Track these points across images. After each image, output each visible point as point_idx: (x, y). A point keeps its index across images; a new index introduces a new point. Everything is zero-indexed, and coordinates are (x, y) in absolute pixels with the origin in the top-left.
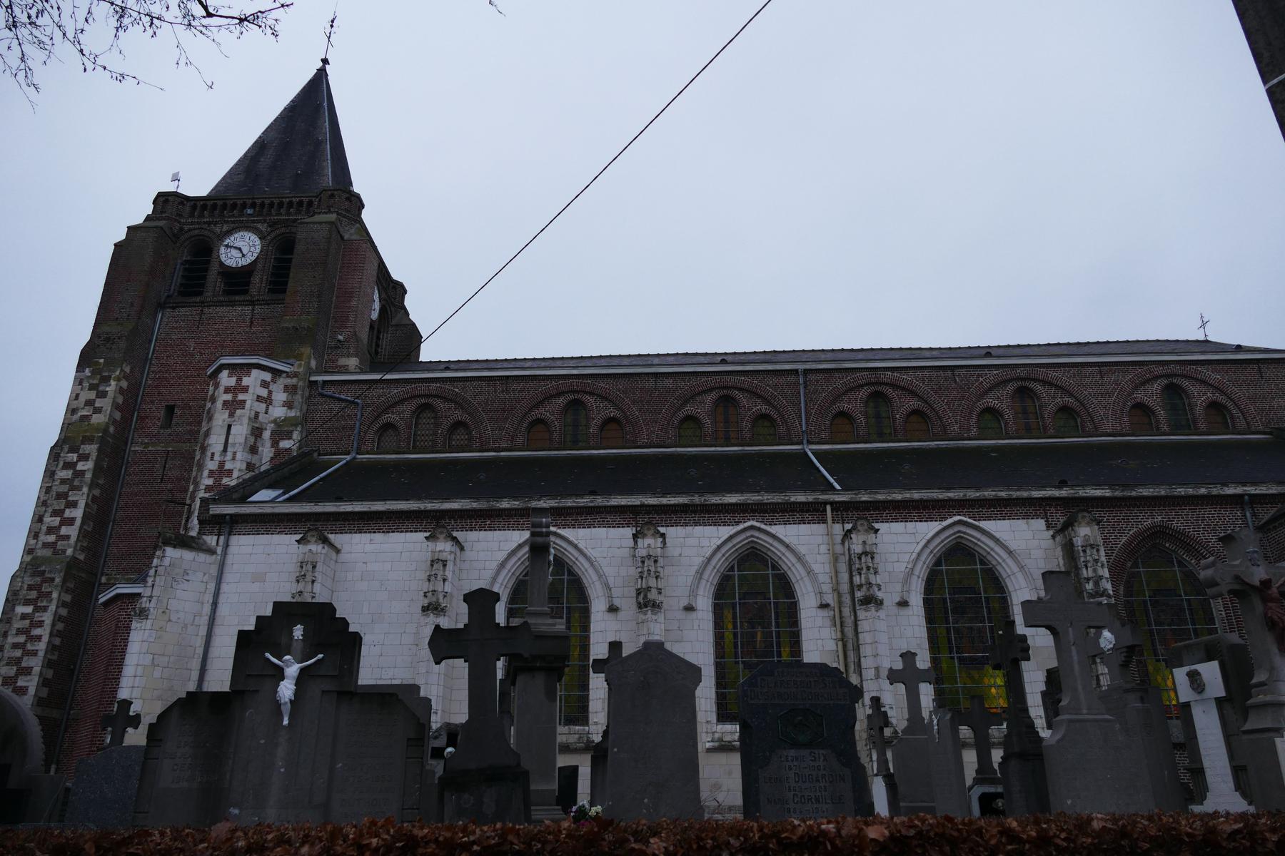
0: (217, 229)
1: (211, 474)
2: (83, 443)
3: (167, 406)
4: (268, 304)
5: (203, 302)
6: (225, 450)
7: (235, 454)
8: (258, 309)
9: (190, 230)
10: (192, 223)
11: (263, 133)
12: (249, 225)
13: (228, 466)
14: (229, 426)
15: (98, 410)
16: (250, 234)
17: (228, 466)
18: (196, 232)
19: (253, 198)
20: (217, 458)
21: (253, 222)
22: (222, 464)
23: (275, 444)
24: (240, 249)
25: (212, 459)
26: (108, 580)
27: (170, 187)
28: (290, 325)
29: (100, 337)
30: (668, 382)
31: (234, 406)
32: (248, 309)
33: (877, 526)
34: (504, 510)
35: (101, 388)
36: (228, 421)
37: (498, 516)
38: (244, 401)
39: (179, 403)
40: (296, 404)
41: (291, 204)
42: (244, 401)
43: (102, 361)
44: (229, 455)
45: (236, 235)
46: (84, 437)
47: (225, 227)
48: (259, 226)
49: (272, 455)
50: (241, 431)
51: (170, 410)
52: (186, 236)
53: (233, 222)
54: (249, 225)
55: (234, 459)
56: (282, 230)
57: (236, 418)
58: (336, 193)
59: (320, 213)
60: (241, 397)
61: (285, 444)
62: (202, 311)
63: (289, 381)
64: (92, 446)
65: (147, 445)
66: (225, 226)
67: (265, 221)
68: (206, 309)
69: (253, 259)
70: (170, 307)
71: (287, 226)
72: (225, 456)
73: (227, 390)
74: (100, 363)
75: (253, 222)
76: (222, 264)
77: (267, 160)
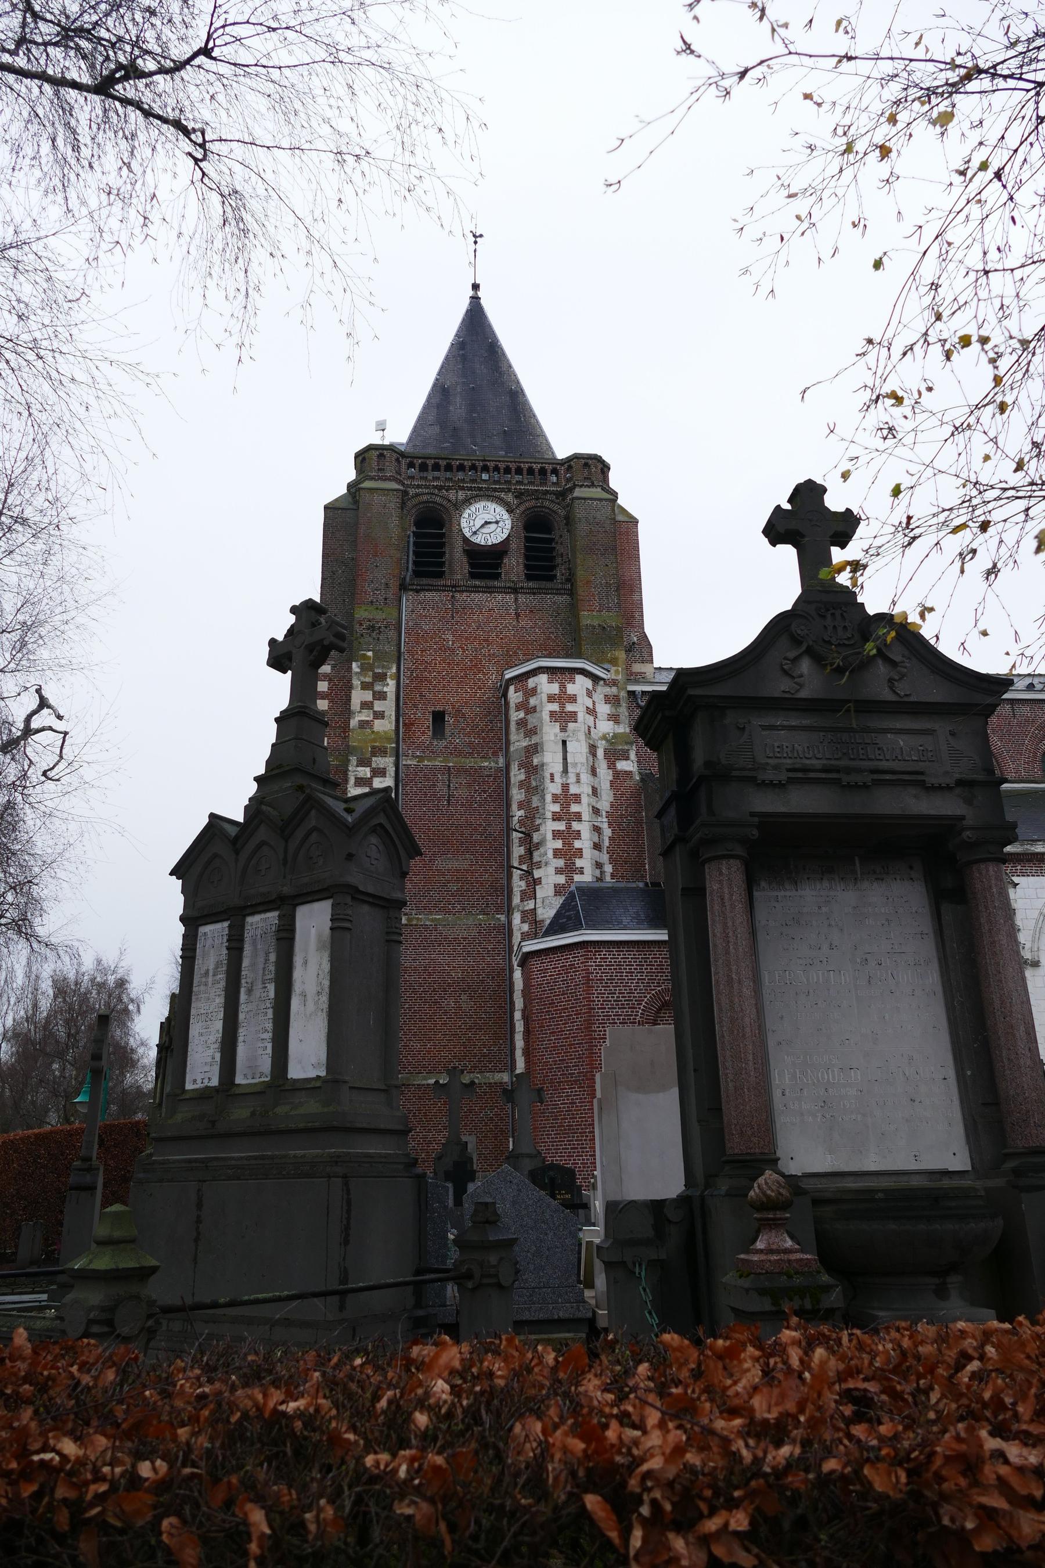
0: (452, 495)
1: (556, 798)
2: (374, 754)
3: (433, 712)
4: (534, 594)
5: (454, 586)
6: (565, 771)
7: (578, 775)
8: (522, 598)
9: (417, 495)
10: (418, 487)
11: (439, 374)
12: (490, 493)
13: (573, 790)
14: (564, 743)
15: (379, 715)
16: (494, 505)
17: (573, 790)
18: (425, 498)
19: (485, 460)
20: (558, 779)
21: (495, 490)
22: (565, 787)
23: (611, 765)
24: (487, 523)
25: (552, 780)
26: (409, 920)
27: (376, 439)
28: (596, 623)
29: (361, 625)
30: (1025, 710)
31: (564, 718)
32: (510, 598)
33: (1016, 879)
34: (1038, 854)
35: (377, 688)
36: (562, 736)
37: (1029, 861)
38: (575, 713)
39: (449, 709)
40: (622, 718)
41: (531, 471)
42: (575, 713)
43: (370, 654)
44: (572, 779)
45: (477, 505)
46: (373, 748)
47: (461, 495)
48: (502, 495)
49: (611, 778)
50: (578, 749)
51: (439, 718)
52: (415, 501)
53: (470, 489)
54: (490, 493)
55: (578, 781)
56: (533, 503)
57: (569, 733)
58: (590, 462)
59: (581, 486)
60: (570, 707)
61: (622, 765)
62: (453, 597)
63: (608, 690)
64: (387, 759)
65: (421, 759)
66: (460, 493)
67: (509, 490)
68: (457, 595)
69: (505, 536)
70: (412, 590)
71: (537, 499)
72: (567, 778)
73: (551, 698)
74: (369, 658)
75: (495, 490)
76: (466, 540)
77: (458, 410)
